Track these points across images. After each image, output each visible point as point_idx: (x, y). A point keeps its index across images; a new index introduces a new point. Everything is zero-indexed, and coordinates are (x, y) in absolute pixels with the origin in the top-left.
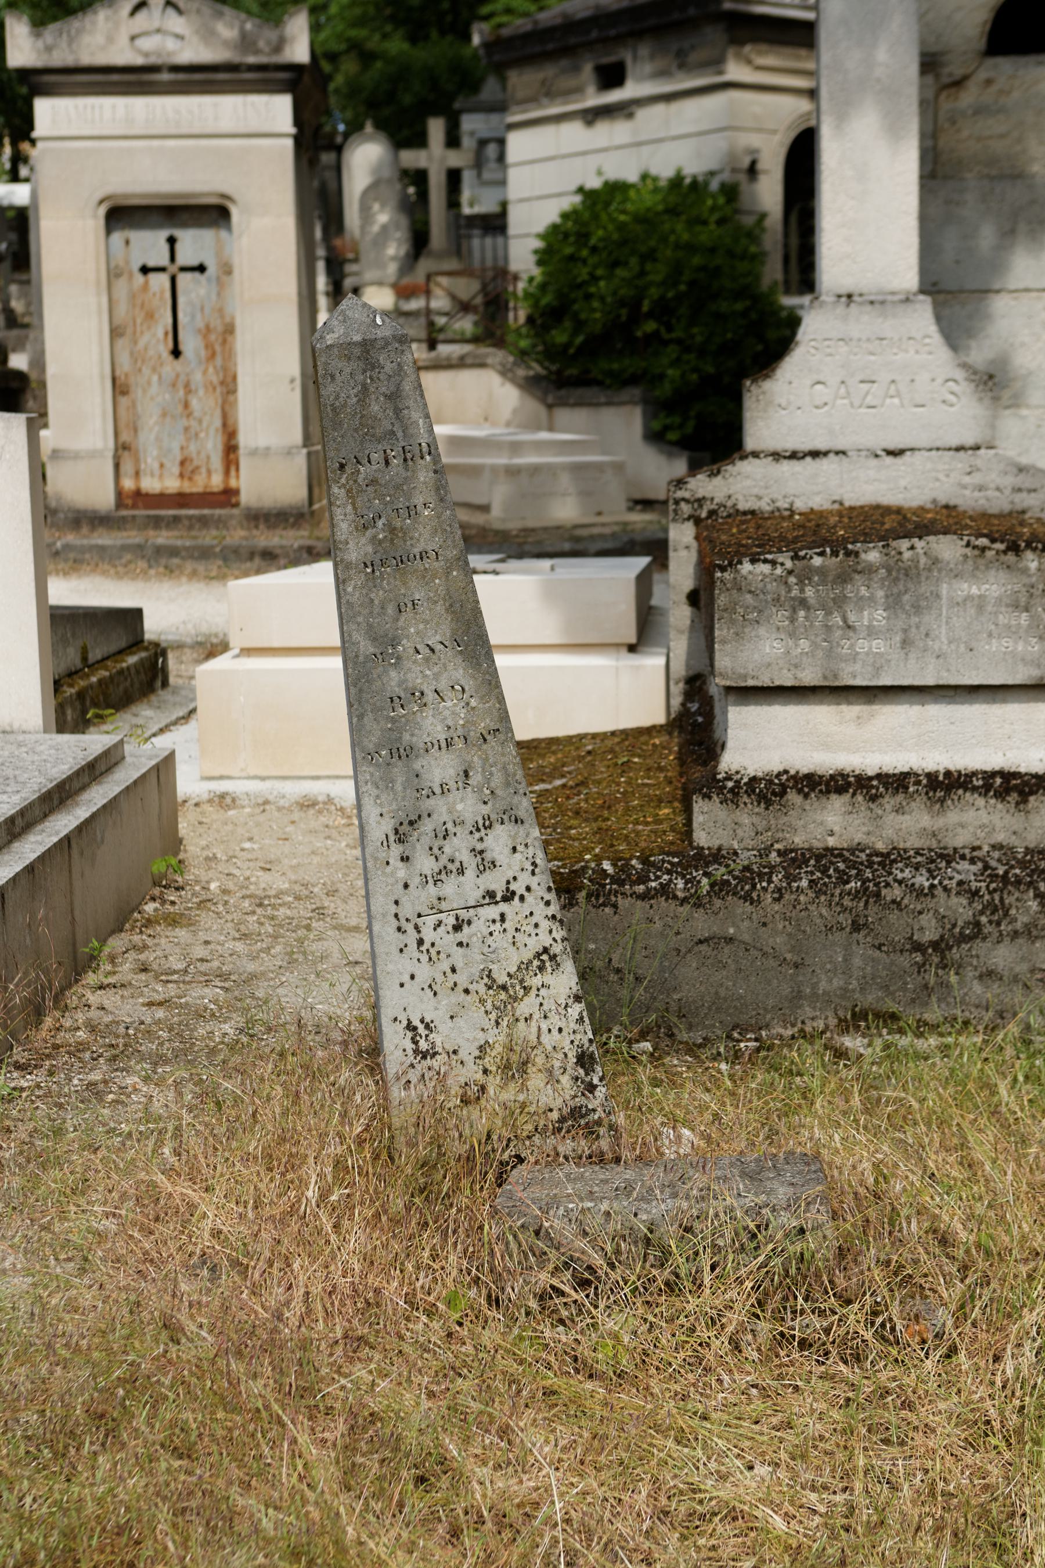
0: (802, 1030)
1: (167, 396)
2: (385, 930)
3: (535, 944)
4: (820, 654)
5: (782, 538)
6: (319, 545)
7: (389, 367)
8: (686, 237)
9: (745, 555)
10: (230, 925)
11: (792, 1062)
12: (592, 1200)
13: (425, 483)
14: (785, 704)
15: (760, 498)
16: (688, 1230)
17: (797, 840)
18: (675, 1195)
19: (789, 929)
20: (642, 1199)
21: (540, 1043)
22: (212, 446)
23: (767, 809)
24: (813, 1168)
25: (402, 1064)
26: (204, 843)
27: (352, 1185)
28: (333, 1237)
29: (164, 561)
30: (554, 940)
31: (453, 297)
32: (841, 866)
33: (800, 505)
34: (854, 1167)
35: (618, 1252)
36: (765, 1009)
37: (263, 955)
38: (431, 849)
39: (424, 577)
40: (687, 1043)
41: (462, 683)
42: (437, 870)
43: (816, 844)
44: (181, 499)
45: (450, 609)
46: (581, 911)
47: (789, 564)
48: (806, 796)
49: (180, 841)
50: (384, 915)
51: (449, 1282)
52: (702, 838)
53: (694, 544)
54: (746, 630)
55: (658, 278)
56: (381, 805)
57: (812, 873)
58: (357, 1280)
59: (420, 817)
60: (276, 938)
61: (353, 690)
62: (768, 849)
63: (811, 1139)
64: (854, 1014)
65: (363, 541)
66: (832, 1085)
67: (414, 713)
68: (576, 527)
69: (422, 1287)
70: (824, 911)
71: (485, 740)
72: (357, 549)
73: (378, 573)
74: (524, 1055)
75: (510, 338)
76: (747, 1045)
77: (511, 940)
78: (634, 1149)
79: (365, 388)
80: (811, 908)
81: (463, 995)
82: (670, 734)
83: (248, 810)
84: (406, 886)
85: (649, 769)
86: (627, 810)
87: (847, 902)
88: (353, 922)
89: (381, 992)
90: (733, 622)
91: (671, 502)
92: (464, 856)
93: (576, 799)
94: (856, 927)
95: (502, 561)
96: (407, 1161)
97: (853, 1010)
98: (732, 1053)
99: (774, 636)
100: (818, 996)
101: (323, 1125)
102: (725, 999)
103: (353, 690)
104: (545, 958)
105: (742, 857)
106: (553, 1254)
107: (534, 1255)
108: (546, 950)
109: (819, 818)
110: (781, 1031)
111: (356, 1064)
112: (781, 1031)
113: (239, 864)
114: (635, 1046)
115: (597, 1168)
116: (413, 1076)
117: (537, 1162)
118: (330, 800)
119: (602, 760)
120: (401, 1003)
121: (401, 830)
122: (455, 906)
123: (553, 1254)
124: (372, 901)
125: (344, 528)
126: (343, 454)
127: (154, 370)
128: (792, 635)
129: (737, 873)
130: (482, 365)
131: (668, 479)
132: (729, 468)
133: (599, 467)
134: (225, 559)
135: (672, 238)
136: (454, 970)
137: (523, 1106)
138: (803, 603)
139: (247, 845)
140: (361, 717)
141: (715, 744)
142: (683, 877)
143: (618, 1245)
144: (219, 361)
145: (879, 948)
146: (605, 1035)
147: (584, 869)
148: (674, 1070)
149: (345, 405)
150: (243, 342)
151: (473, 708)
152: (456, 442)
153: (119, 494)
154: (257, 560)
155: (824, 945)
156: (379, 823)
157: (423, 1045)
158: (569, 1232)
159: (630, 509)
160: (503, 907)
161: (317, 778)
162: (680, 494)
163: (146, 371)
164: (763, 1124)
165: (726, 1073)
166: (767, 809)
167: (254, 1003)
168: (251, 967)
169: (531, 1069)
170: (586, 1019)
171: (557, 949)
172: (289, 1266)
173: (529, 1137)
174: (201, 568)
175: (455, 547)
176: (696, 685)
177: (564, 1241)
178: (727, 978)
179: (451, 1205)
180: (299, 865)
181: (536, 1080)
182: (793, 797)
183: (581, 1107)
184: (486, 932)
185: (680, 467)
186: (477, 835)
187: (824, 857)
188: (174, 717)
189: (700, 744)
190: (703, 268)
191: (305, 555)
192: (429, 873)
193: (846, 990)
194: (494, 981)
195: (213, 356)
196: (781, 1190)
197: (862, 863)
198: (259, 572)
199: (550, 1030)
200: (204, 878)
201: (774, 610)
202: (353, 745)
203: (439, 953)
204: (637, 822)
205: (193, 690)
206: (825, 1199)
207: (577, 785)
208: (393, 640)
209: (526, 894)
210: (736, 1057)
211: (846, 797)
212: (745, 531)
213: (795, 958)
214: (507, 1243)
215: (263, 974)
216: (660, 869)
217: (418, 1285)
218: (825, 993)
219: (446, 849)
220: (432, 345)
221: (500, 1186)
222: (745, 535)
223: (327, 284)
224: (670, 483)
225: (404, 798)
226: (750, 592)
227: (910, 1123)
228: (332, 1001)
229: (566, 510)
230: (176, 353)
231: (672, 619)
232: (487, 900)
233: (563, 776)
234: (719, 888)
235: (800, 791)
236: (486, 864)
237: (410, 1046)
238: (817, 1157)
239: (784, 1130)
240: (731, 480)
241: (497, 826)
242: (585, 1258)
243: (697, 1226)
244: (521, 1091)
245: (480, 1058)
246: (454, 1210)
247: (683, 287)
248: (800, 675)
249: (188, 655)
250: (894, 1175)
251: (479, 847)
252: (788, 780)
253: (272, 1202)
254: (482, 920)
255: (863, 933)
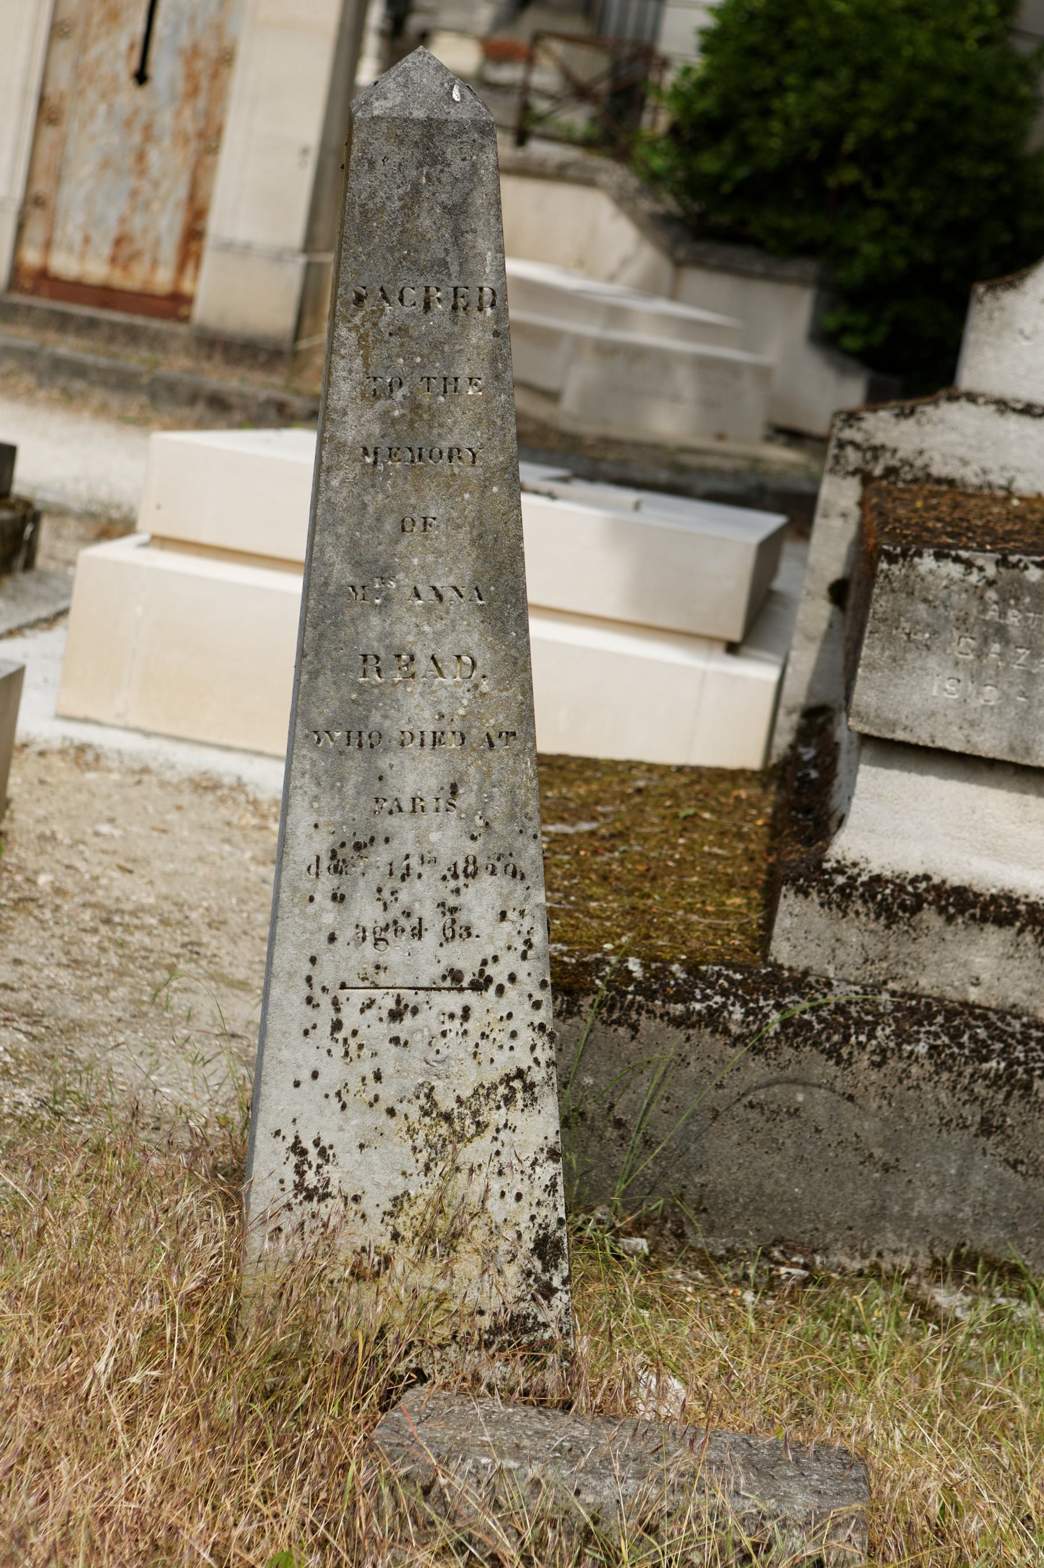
0: (875, 1266)
1: (116, 139)
2: (289, 998)
3: (505, 1062)
4: (1011, 712)
5: (988, 530)
6: (298, 404)
7: (458, 166)
8: (928, 53)
9: (928, 544)
10: (56, 942)
11: (852, 1311)
12: (516, 1459)
13: (478, 347)
14: (946, 777)
15: (965, 463)
16: (651, 1530)
17: (923, 982)
18: (641, 1475)
19: (886, 1112)
20: (591, 1471)
21: (483, 1209)
22: (167, 225)
23: (888, 927)
24: (854, 1474)
25: (274, 1201)
26: (41, 812)
27: (165, 1365)
28: (122, 1438)
29: (64, 381)
30: (536, 1061)
31: (567, 74)
32: (982, 1033)
33: (1024, 485)
34: (915, 1485)
35: (541, 1542)
36: (828, 1225)
37: (97, 997)
38: (379, 890)
39: (449, 486)
40: (701, 1251)
41: (475, 654)
42: (382, 924)
43: (951, 994)
44: (106, 295)
45: (478, 541)
46: (584, 1028)
47: (991, 571)
48: (950, 919)
49: (7, 803)
50: (291, 975)
51: (282, 1537)
52: (783, 951)
53: (855, 513)
54: (909, 656)
55: (874, 105)
56: (318, 811)
57: (936, 1036)
58: (146, 1509)
59: (372, 840)
60: (121, 974)
61: (310, 633)
62: (878, 987)
63: (859, 1431)
64: (957, 1257)
65: (369, 414)
66: (906, 1356)
67: (394, 685)
68: (684, 450)
69: (240, 1538)
70: (943, 1095)
71: (492, 745)
72: (358, 426)
73: (381, 467)
74: (457, 1223)
75: (640, 151)
76: (791, 1272)
77: (471, 1049)
78: (594, 1395)
79: (416, 189)
80: (927, 1087)
81: (384, 1116)
82: (765, 786)
83: (115, 777)
84: (332, 938)
85: (723, 833)
86: (680, 889)
87: (979, 1088)
88: (240, 974)
89: (264, 1089)
90: (891, 640)
91: (833, 443)
92: (427, 911)
93: (606, 857)
94: (986, 1128)
95: (564, 480)
96: (253, 1345)
97: (957, 1251)
98: (765, 1279)
99: (948, 673)
100: (910, 1218)
101: (139, 1267)
102: (771, 1198)
103: (310, 633)
104: (517, 1085)
105: (837, 991)
106: (443, 1527)
107: (415, 1522)
108: (520, 1074)
109: (962, 955)
110: (845, 1260)
111: (205, 1188)
112: (845, 1260)
113: (87, 854)
114: (624, 1240)
115: (533, 1412)
116: (288, 1222)
117: (445, 1386)
118: (240, 786)
119: (656, 806)
120: (290, 1109)
121: (341, 854)
122: (399, 982)
123: (443, 1527)
124: (278, 951)
125: (344, 390)
126: (365, 280)
127: (103, 96)
128: (975, 676)
129: (824, 1014)
130: (588, 182)
131: (835, 408)
132: (929, 409)
133: (733, 368)
134: (153, 396)
135: (907, 52)
136: (378, 1077)
137: (442, 1299)
138: (1001, 632)
139: (105, 829)
140: (314, 675)
141: (830, 816)
142: (744, 1003)
143: (543, 1532)
144: (201, 102)
145: (1014, 1167)
146: (582, 1217)
147: (600, 963)
148: (675, 1288)
149: (382, 209)
150: (243, 80)
151: (483, 695)
152: (538, 293)
153: (16, 268)
154: (200, 408)
155: (933, 1146)
156: (310, 837)
157: (311, 1179)
158: (474, 1499)
159: (768, 439)
160: (469, 997)
161: (228, 749)
162: (848, 434)
163: (91, 95)
164: (792, 1394)
165: (751, 1308)
166: (888, 927)
167: (70, 1066)
168: (77, 1011)
169: (462, 1245)
170: (560, 1188)
171: (537, 1075)
172: (48, 1466)
173: (441, 1347)
174: (115, 401)
175: (503, 450)
176: (817, 721)
177: (464, 1512)
178: (780, 1166)
179: (307, 1425)
180: (176, 873)
181: (467, 1265)
182: (929, 916)
183: (527, 1317)
184: (437, 1029)
185: (853, 392)
186: (452, 884)
187: (959, 1015)
188: (32, 616)
189: (808, 811)
190: (944, 105)
191: (272, 414)
192: (369, 926)
193: (952, 1219)
194: (435, 1104)
195: (193, 92)
196: (800, 1498)
197: (1012, 1035)
198: (200, 425)
199: (503, 1194)
200: (31, 865)
201: (956, 634)
202: (295, 714)
203: (361, 1047)
204: (690, 909)
205: (69, 582)
206: (863, 1524)
207: (612, 836)
208: (385, 570)
209: (507, 985)
210: (771, 1287)
211: (1009, 933)
212: (934, 508)
213: (887, 1157)
214: (379, 1498)
215: (92, 1025)
216: (711, 985)
217: (236, 1533)
218: (920, 1217)
219: (404, 896)
220: (522, 138)
221: (384, 1410)
222: (933, 514)
223: (386, 17)
224: (837, 414)
225: (353, 809)
226: (925, 600)
227: (1010, 1434)
228: (191, 1089)
229: (669, 422)
230: (141, 77)
231: (800, 617)
232: (448, 983)
233: (594, 819)
234: (794, 1030)
235: (942, 910)
236: (457, 930)
237: (291, 1177)
238: (863, 1457)
239: (821, 1410)
240: (928, 428)
241: (485, 877)
242: (490, 1542)
243: (666, 1527)
244: (443, 1275)
245: (391, 1214)
246: (310, 1432)
247: (909, 127)
248: (975, 738)
249: (71, 527)
250: (971, 1507)
251: (452, 901)
252: (927, 890)
253: (41, 1368)
254: (435, 1010)
255: (994, 1139)
